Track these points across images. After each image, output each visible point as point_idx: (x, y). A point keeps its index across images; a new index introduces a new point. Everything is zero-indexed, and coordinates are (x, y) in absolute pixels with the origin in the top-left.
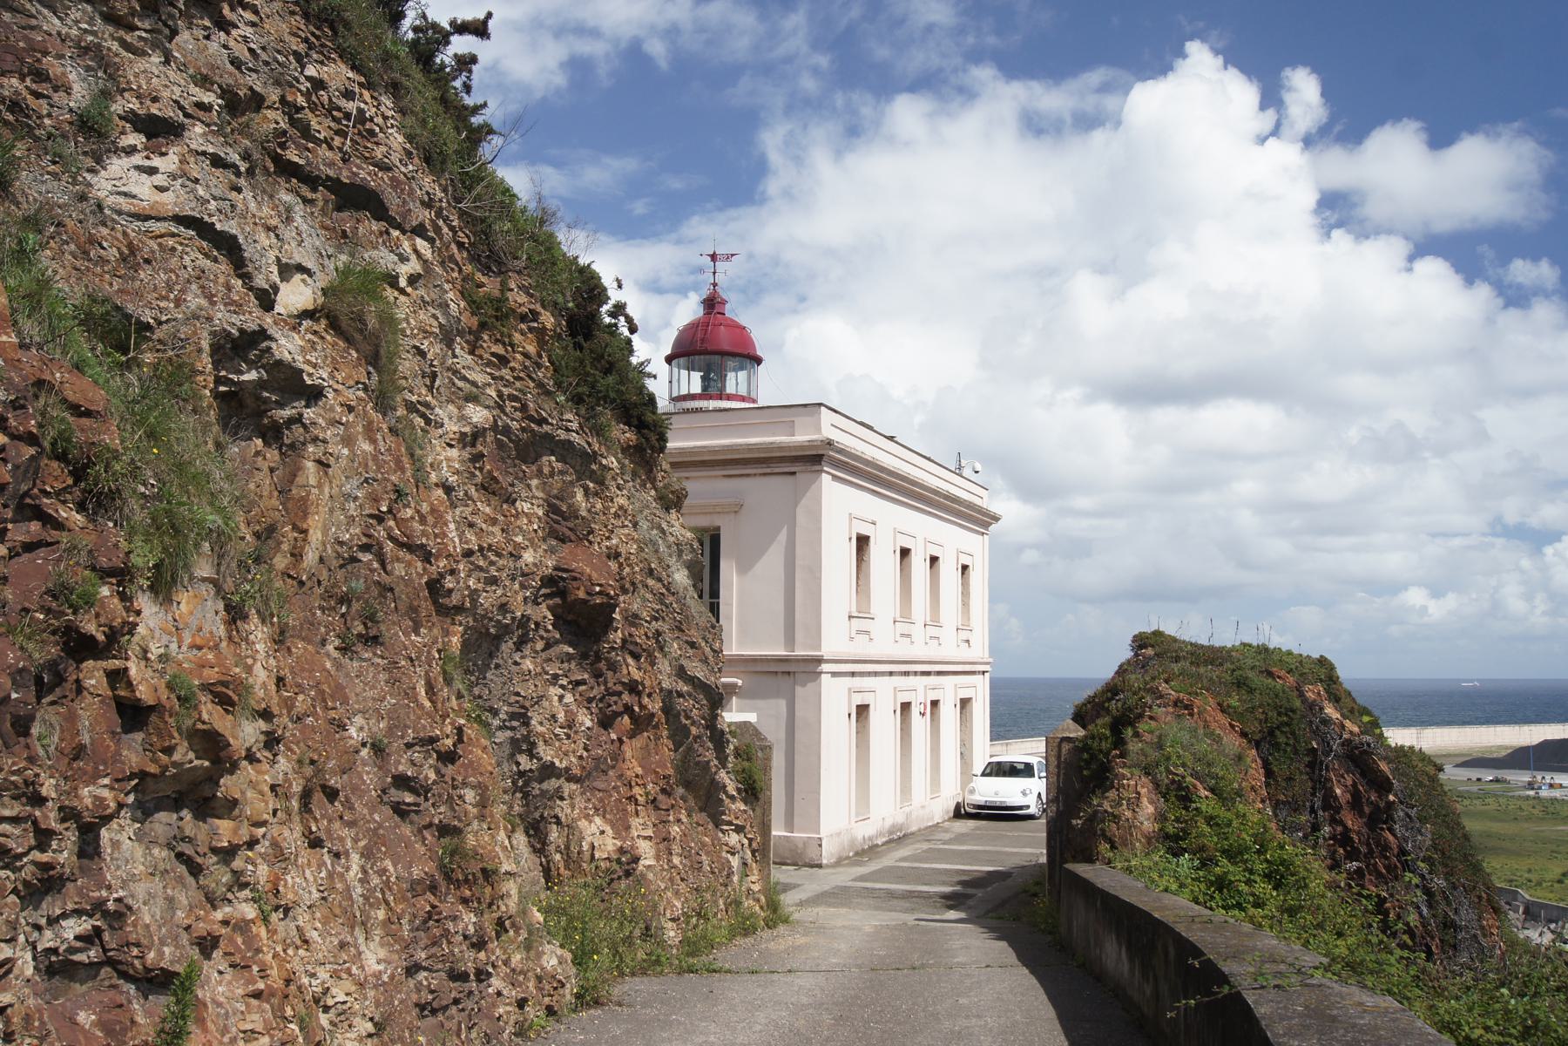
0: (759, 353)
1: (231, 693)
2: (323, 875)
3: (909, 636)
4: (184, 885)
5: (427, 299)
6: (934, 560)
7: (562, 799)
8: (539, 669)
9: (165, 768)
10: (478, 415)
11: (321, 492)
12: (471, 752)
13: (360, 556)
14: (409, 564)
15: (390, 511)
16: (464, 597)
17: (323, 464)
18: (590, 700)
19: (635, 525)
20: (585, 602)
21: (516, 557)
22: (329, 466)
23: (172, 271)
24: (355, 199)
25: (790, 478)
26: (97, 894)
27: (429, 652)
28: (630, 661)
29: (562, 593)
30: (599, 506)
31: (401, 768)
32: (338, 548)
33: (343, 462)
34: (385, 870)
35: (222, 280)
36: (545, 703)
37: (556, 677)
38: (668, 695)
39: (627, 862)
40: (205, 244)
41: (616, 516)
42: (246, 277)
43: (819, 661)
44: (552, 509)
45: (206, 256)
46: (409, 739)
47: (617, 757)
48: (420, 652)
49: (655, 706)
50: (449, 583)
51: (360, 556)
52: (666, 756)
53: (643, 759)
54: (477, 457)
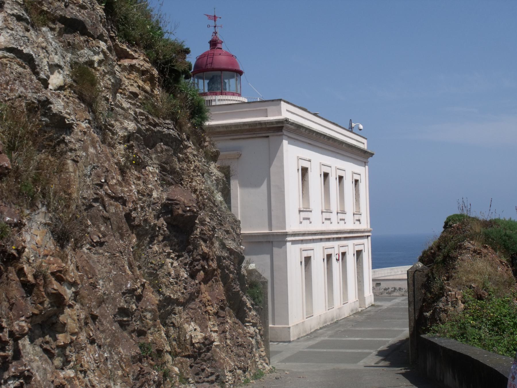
0: (241, 69)
1: (62, 275)
2: (97, 355)
3: (329, 219)
4: (48, 363)
5: (106, 71)
6: (341, 178)
7: (175, 314)
8: (161, 250)
9: (41, 311)
10: (131, 126)
11: (75, 174)
12: (147, 295)
13: (94, 204)
14: (116, 207)
15: (106, 181)
16: (141, 220)
17: (75, 161)
18: (185, 264)
19: (203, 175)
20: (182, 215)
21: (150, 195)
22: (77, 162)
23: (7, 75)
24: (73, 26)
25: (266, 140)
26: (21, 368)
27: (128, 249)
28: (202, 243)
29: (171, 212)
30: (185, 166)
31: (121, 304)
32: (84, 201)
33: (83, 159)
34: (120, 352)
35: (28, 77)
36: (165, 267)
37: (169, 254)
38: (219, 259)
39: (207, 343)
40: (19, 60)
41: (194, 171)
42: (37, 74)
43: (286, 235)
44: (163, 169)
45: (21, 66)
46: (123, 291)
47: (199, 292)
48: (125, 249)
49: (214, 265)
50: (134, 214)
51: (94, 204)
52: (220, 288)
53: (213, 293)
54: (130, 147)
